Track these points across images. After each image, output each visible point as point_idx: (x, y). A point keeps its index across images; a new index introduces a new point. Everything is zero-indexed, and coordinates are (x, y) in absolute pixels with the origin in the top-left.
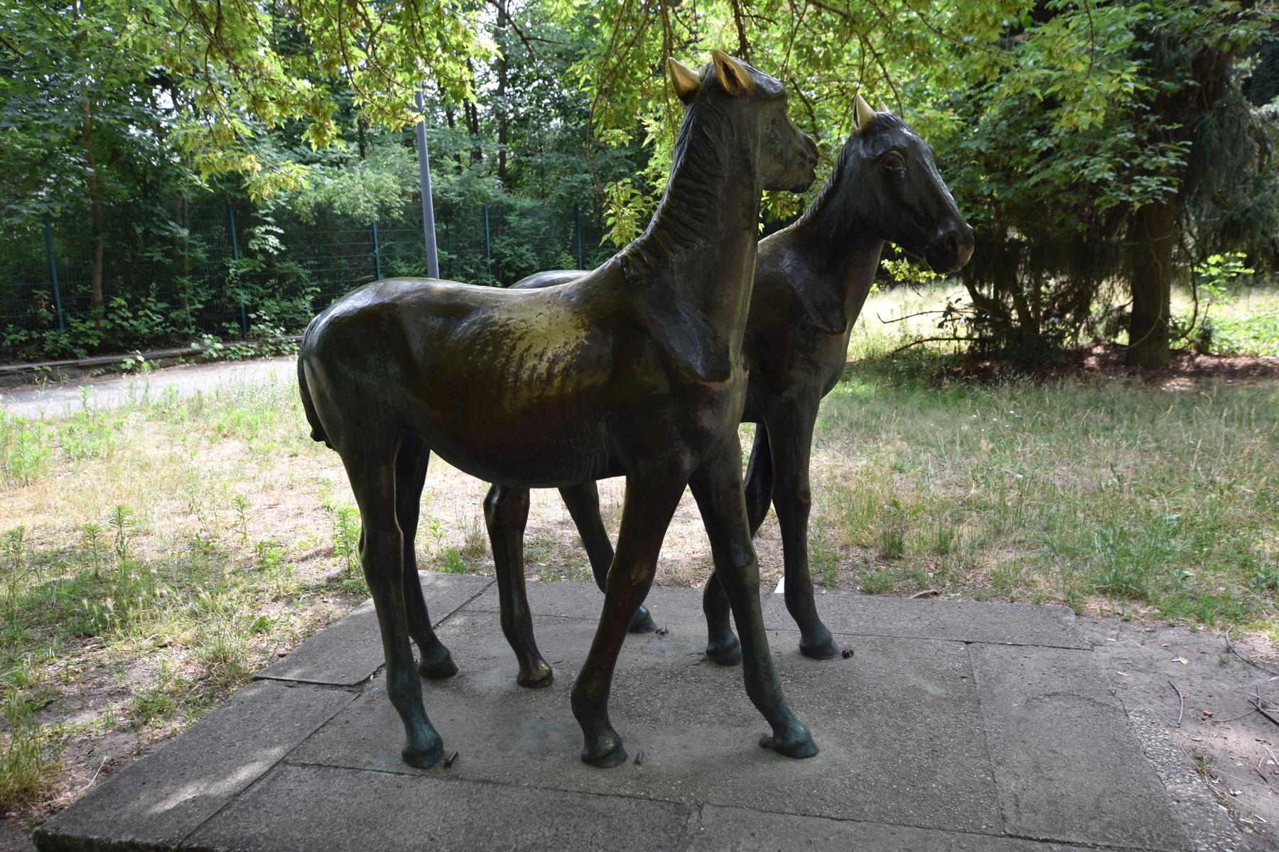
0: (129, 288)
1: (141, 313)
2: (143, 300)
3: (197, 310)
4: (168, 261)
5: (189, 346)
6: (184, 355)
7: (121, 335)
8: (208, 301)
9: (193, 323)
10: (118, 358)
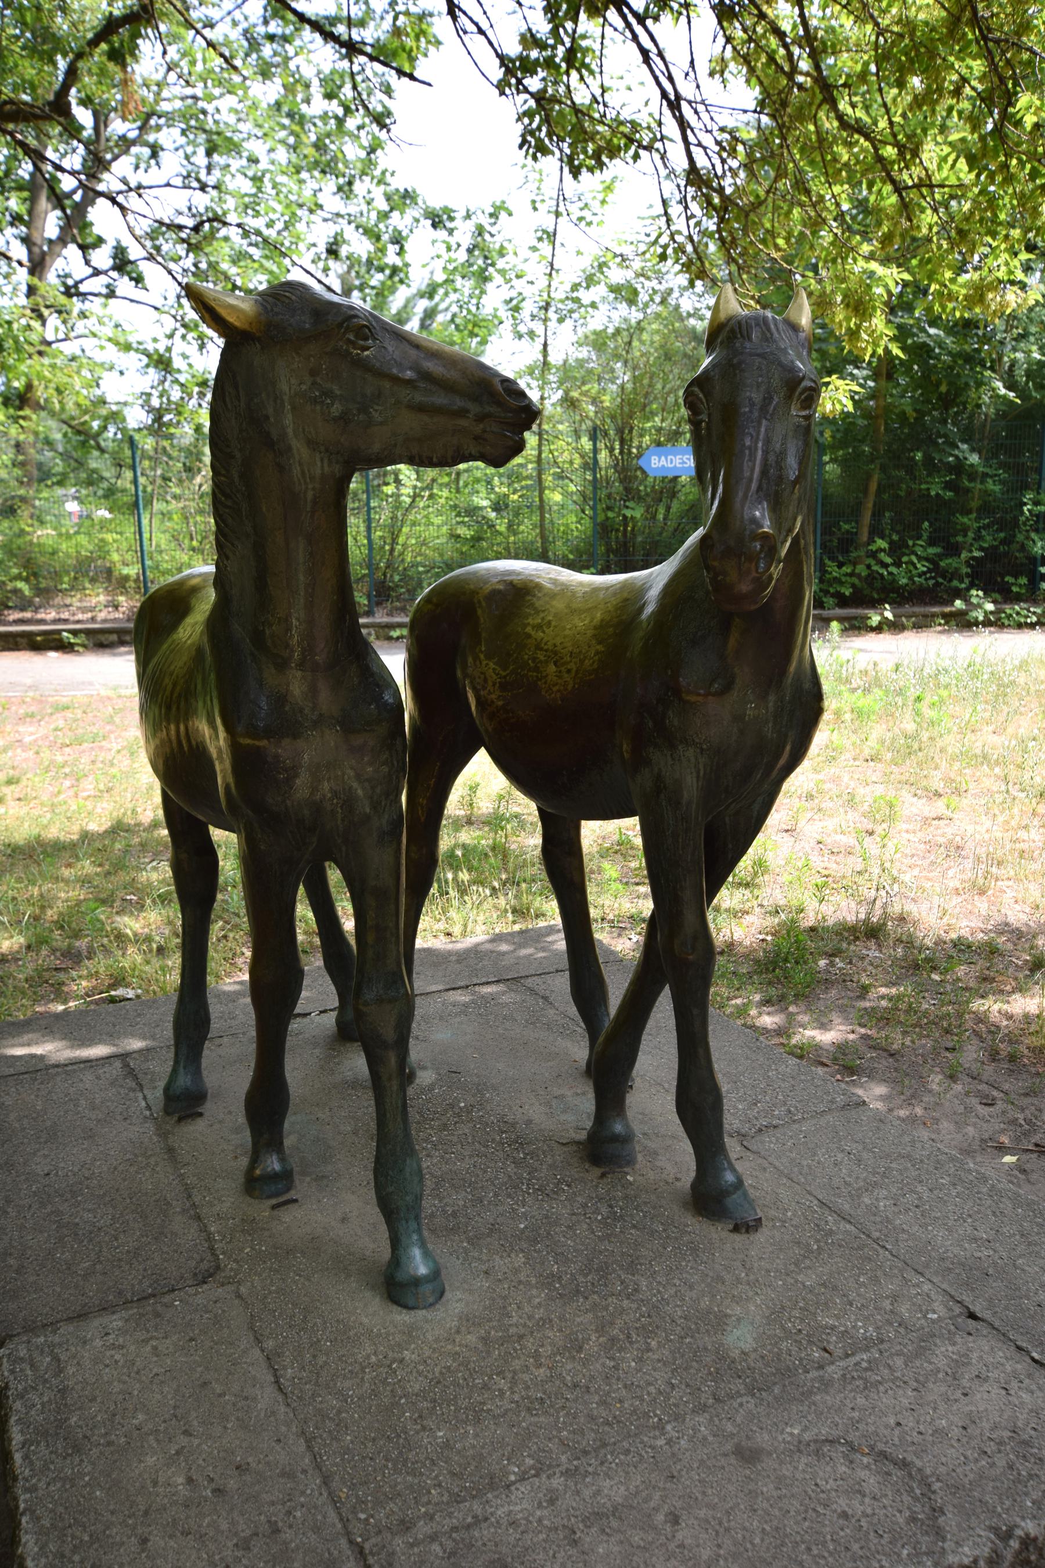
0: (899, 527)
1: (905, 559)
2: (910, 543)
3: (974, 558)
4: (949, 494)
5: (952, 605)
6: (944, 616)
7: (878, 584)
8: (992, 547)
9: (968, 575)
10: (860, 611)
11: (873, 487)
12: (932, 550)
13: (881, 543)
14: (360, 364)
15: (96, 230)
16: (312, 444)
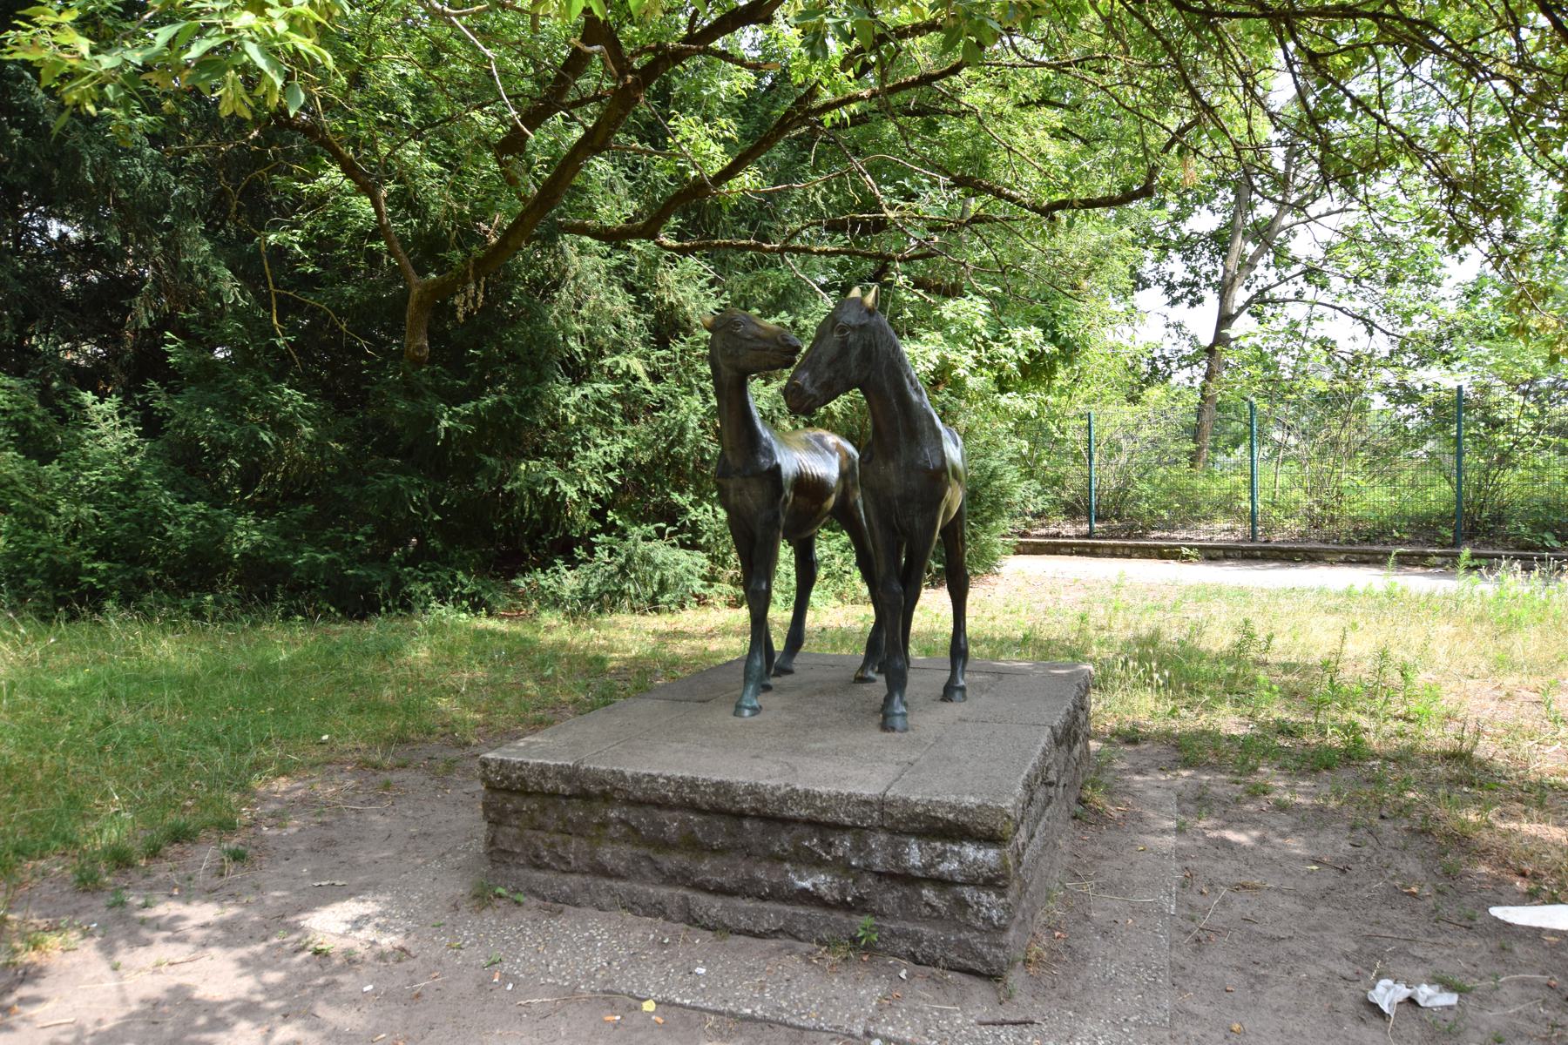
14: (735, 335)
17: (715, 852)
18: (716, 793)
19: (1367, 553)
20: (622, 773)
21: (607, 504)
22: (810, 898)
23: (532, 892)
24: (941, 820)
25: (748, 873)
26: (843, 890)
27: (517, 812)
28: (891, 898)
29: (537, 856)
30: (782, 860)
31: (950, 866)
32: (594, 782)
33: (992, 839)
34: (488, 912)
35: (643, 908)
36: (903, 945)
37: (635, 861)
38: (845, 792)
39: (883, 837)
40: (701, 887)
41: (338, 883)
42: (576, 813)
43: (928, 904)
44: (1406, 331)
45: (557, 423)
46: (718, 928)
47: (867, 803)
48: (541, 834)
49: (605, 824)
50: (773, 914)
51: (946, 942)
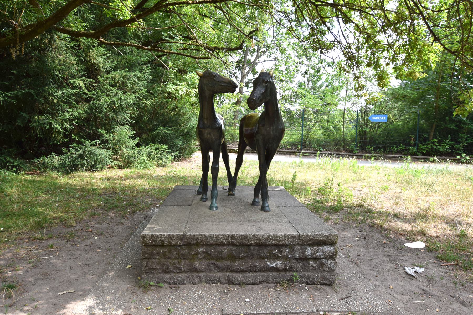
10: (428, 157)
11: (434, 126)
12: (451, 143)
13: (435, 140)
14: (214, 80)
15: (256, 70)
16: (208, 90)
17: (239, 258)
18: (242, 239)
19: (282, 151)
20: (205, 235)
21: (71, 131)
22: (275, 269)
23: (165, 282)
24: (318, 240)
25: (252, 264)
26: (285, 266)
27: (158, 253)
28: (299, 266)
29: (167, 269)
30: (264, 258)
31: (320, 254)
32: (193, 239)
33: (332, 244)
34: (150, 292)
35: (212, 281)
36: (304, 280)
37: (208, 265)
38: (287, 234)
39: (299, 247)
40: (235, 271)
41: (71, 291)
42: (185, 251)
43: (312, 266)
44: (284, 94)
45: (50, 103)
46: (241, 284)
47: (295, 237)
48: (169, 260)
49: (196, 254)
50: (260, 276)
51: (318, 276)
